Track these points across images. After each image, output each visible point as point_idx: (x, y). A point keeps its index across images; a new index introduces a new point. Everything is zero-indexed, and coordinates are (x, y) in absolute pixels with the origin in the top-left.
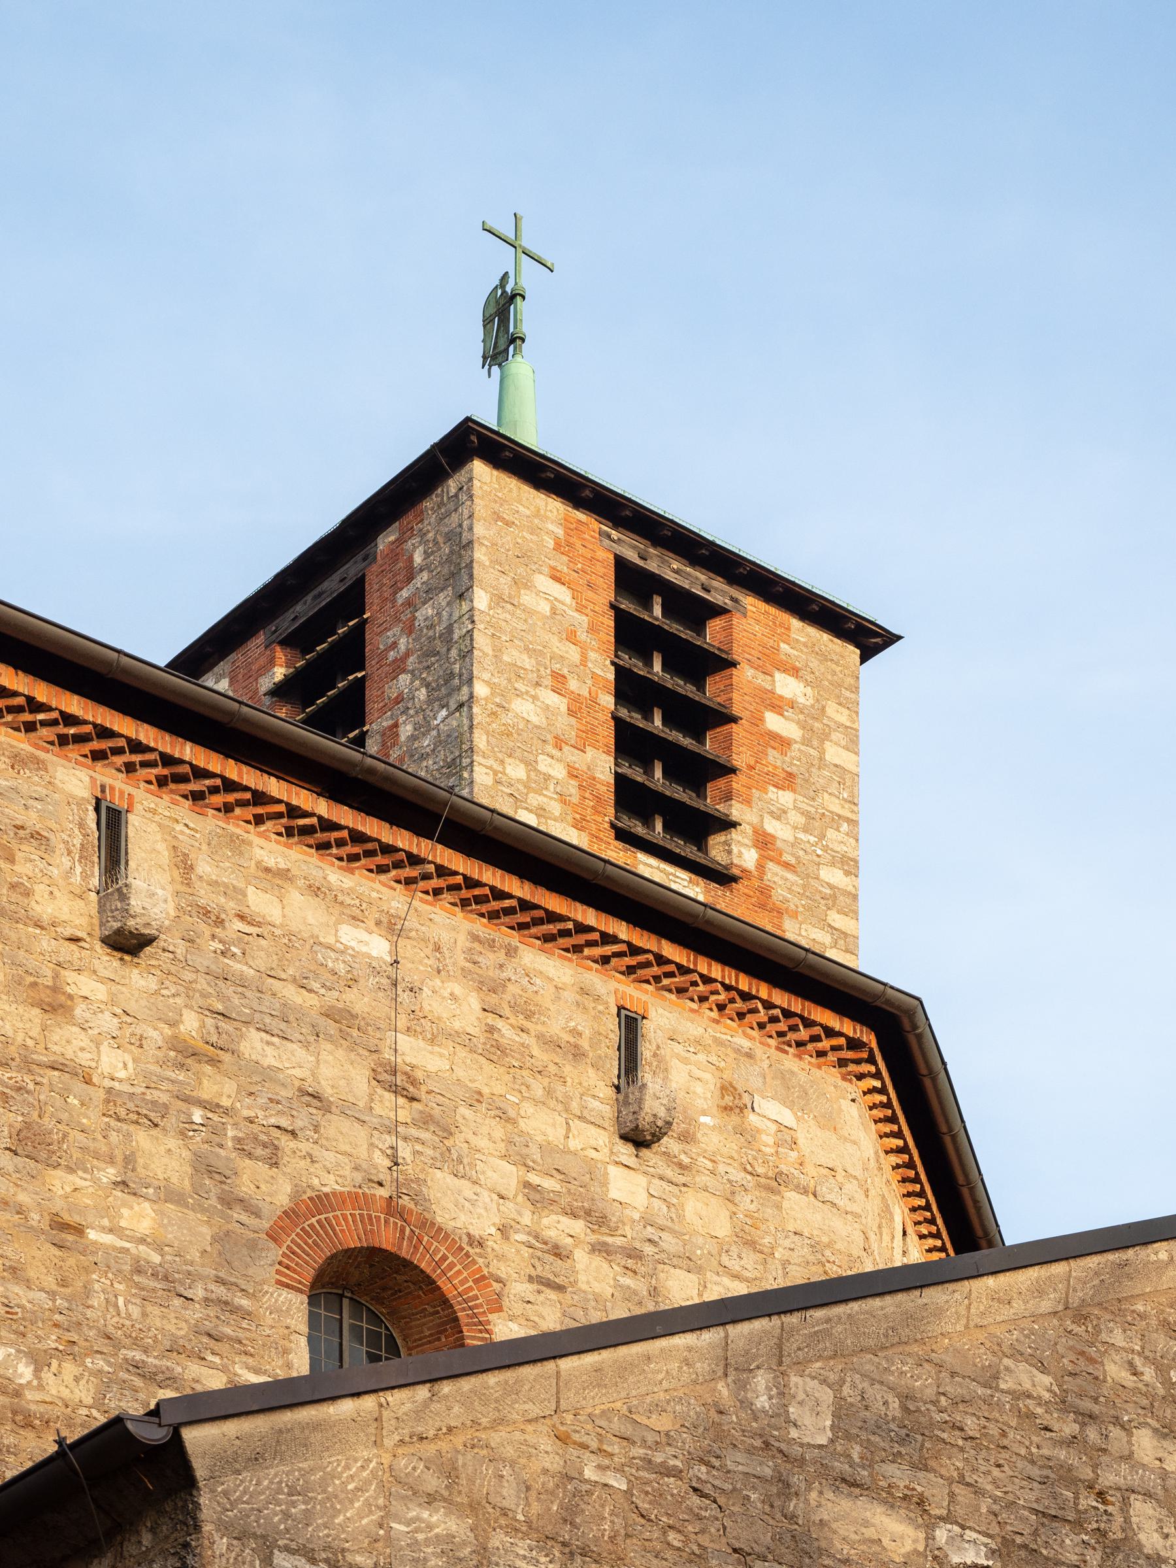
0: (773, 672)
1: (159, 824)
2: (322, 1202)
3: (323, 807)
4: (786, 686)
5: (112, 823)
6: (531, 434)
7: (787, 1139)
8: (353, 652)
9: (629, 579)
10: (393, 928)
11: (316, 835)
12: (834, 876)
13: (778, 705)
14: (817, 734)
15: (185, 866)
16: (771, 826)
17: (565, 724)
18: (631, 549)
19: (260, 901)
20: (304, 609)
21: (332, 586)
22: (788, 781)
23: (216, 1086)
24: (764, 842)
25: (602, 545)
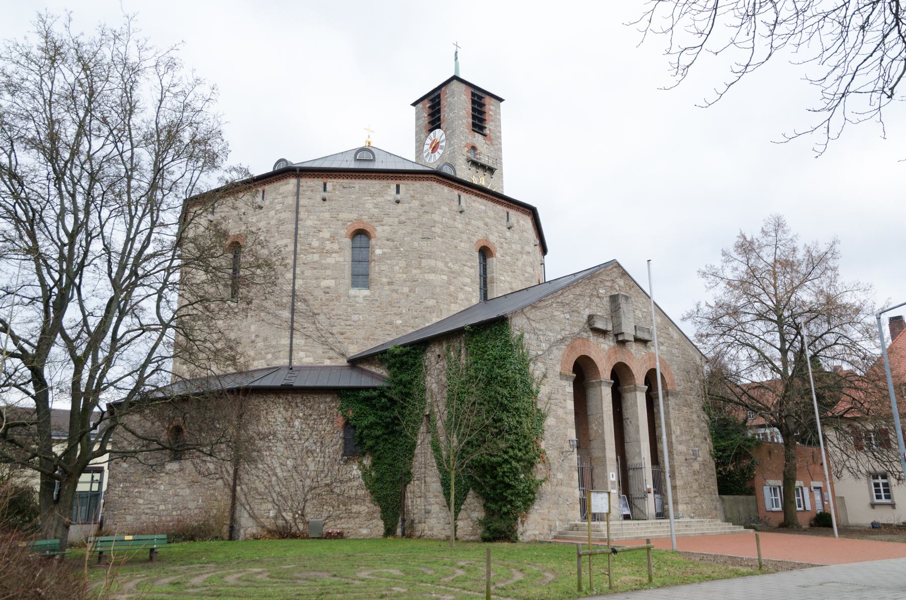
0: (490, 105)
4: (492, 107)
5: (459, 197)
6: (462, 76)
8: (439, 103)
9: (473, 94)
11: (477, 195)
14: (496, 114)
19: (473, 204)
20: (432, 96)
21: (436, 94)
23: (470, 228)
25: (470, 90)
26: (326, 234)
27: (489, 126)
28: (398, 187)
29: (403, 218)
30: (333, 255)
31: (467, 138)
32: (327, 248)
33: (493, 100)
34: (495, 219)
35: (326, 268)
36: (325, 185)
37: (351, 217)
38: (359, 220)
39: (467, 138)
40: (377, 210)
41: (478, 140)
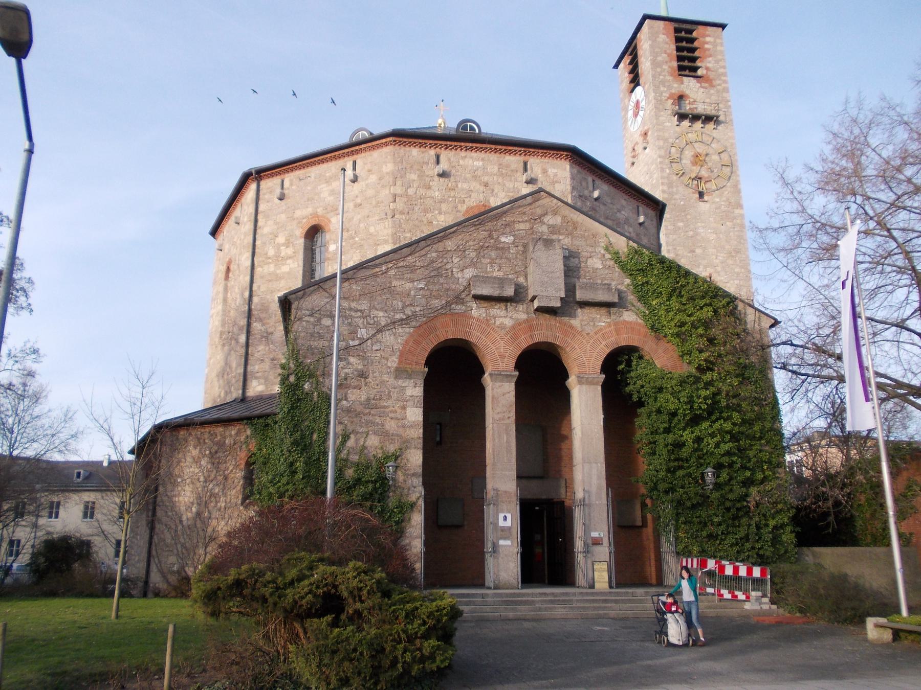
0: (707, 39)
1: (445, 155)
2: (472, 208)
3: (471, 145)
7: (556, 175)
9: (677, 30)
10: (483, 160)
12: (721, 70)
13: (707, 43)
14: (715, 45)
15: (449, 160)
16: (709, 65)
17: (667, 59)
18: (677, 25)
22: (710, 56)
24: (707, 69)
26: (281, 239)
27: (705, 65)
28: (355, 163)
29: (359, 201)
30: (289, 261)
31: (670, 87)
32: (283, 254)
33: (710, 29)
34: (502, 175)
35: (281, 278)
36: (283, 181)
37: (305, 215)
38: (315, 215)
39: (670, 87)
40: (332, 198)
41: (689, 85)
